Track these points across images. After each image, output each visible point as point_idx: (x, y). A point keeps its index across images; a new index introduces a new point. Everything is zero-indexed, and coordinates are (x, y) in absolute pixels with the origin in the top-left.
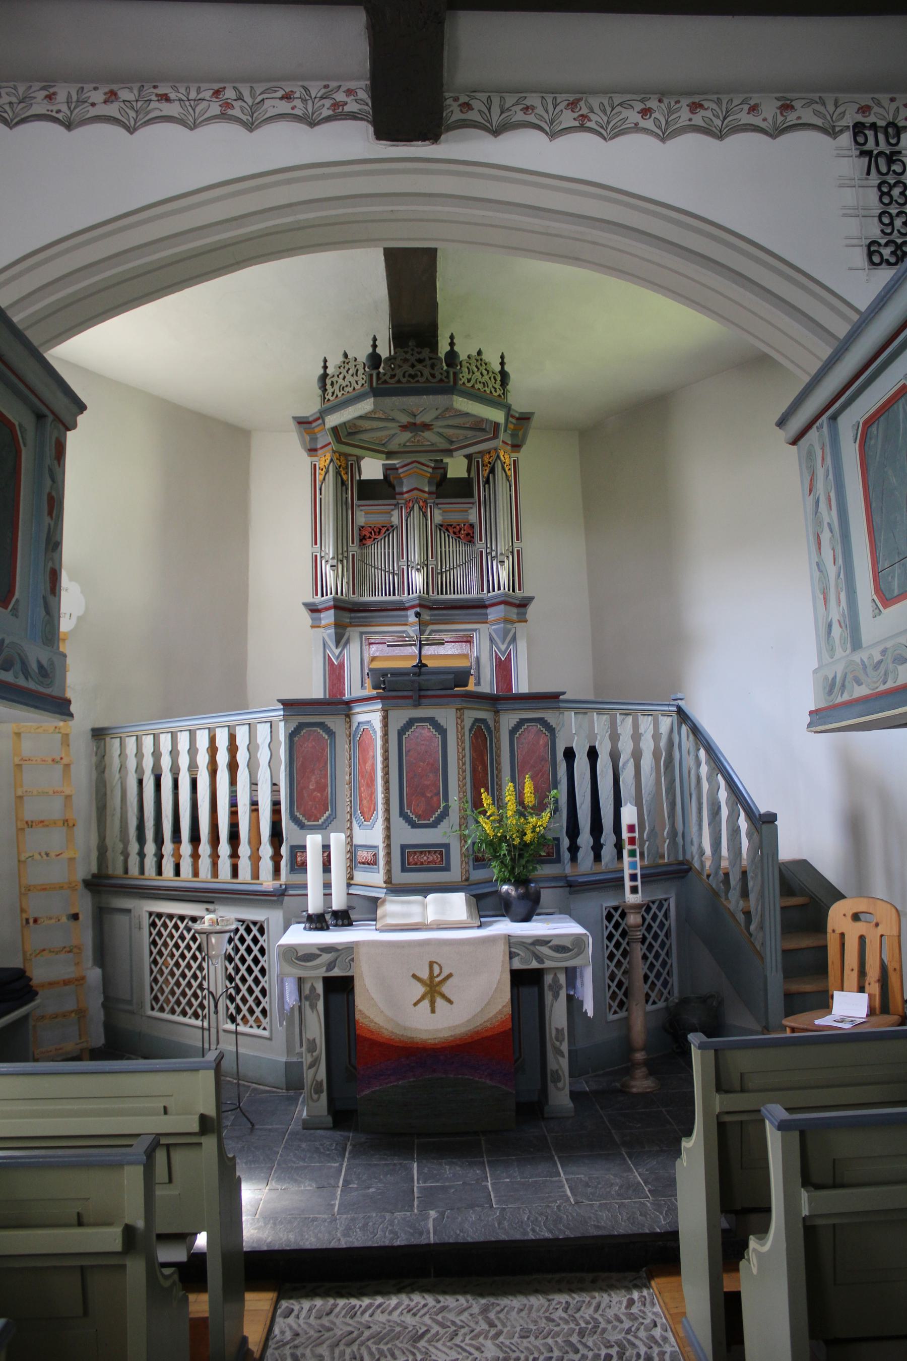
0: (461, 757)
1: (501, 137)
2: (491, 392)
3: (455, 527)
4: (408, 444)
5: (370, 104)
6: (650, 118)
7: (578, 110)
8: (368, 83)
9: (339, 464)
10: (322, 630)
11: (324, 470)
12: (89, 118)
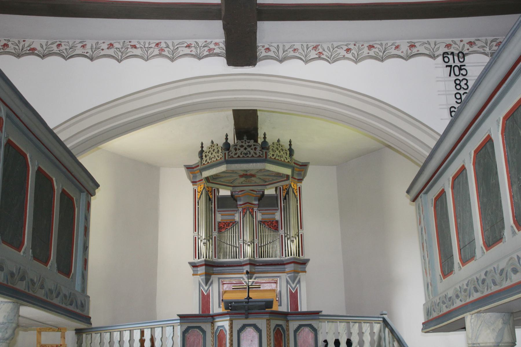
0: (269, 344)
1: (283, 63)
2: (284, 160)
3: (268, 222)
4: (244, 182)
5: (225, 50)
6: (350, 53)
7: (318, 50)
8: (224, 40)
9: (208, 190)
10: (198, 276)
11: (200, 192)
12: (100, 56)
